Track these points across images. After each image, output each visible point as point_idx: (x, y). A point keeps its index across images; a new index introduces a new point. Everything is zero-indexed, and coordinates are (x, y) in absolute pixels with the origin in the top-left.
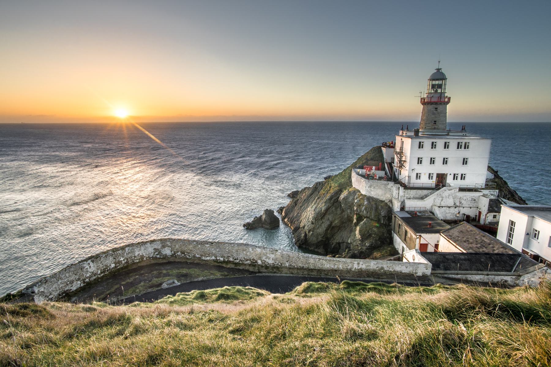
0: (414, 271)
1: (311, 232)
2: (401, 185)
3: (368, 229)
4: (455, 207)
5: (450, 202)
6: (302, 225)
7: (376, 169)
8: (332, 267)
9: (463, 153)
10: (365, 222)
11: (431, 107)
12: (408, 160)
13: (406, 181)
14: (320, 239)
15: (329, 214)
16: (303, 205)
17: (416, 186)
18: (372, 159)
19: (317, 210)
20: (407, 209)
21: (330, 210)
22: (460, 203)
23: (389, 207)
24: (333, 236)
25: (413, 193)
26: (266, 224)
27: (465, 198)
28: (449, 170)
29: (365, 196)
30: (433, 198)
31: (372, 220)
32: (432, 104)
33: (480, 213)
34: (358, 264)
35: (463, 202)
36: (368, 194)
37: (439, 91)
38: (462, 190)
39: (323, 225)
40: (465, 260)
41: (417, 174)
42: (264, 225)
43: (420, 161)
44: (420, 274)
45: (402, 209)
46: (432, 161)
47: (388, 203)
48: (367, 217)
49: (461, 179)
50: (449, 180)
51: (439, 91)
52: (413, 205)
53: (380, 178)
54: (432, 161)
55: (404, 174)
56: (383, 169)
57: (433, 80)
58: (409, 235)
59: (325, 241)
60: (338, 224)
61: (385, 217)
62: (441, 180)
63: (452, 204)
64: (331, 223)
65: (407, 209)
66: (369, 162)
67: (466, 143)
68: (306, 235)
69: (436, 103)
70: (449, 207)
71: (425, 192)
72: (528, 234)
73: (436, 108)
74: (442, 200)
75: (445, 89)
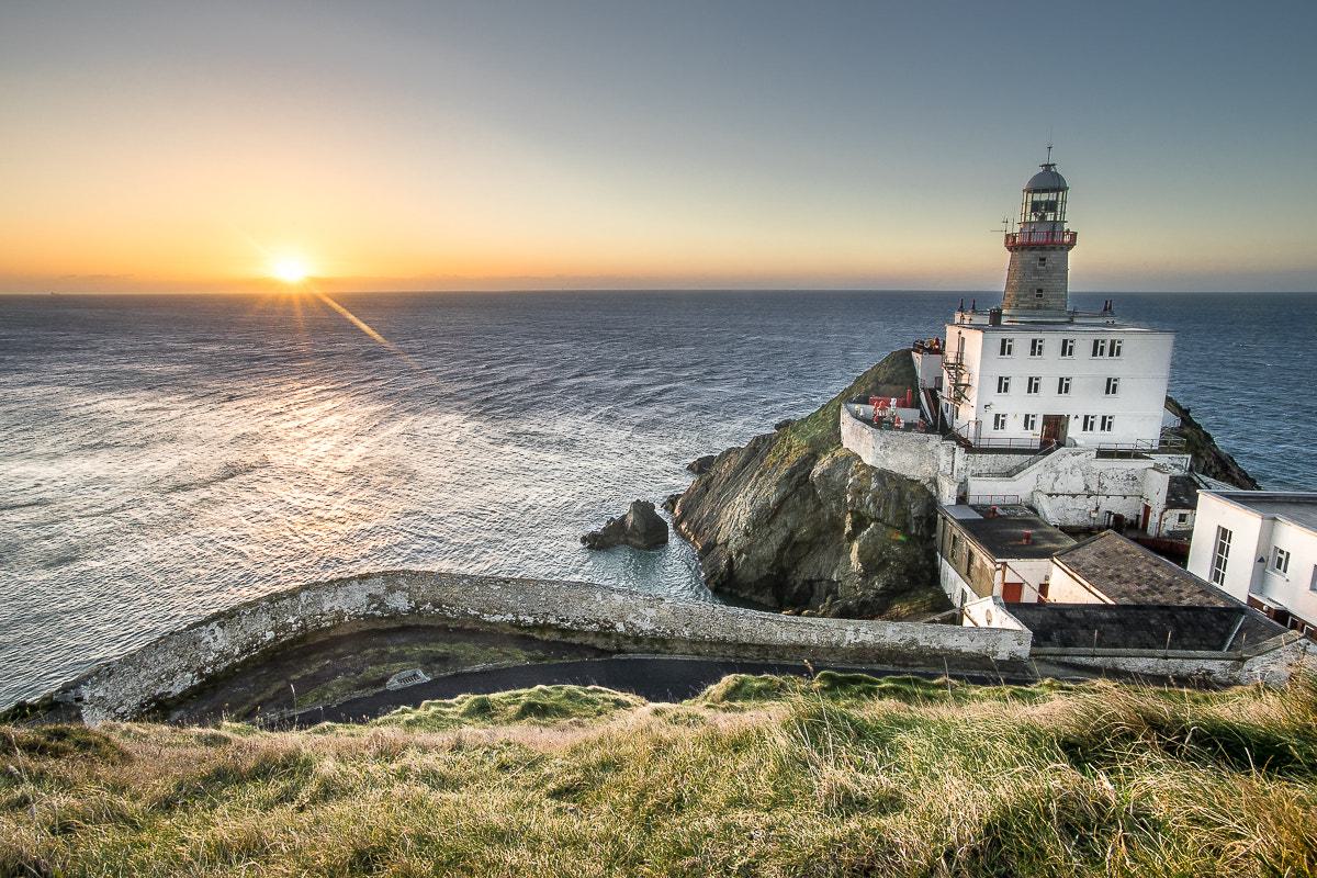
0: (990, 649)
3: (879, 546)
4: (1089, 496)
5: (1076, 483)
6: (721, 538)
7: (898, 405)
9: (1107, 367)
11: (1029, 256)
14: (765, 571)
15: (787, 513)
17: (993, 444)
19: (758, 503)
20: (972, 501)
21: (790, 503)
22: (1100, 485)
25: (986, 461)
26: (635, 536)
30: (1036, 472)
31: (888, 525)
33: (1147, 509)
34: (857, 631)
35: (1107, 482)
36: (879, 465)
38: (1103, 454)
39: (772, 538)
41: (997, 416)
42: (630, 539)
43: (1003, 385)
44: (1003, 655)
45: (962, 499)
46: (1033, 386)
47: (928, 487)
48: (876, 520)
50: (1074, 430)
51: (1050, 217)
52: (987, 490)
53: (909, 427)
54: (1033, 386)
55: (966, 417)
56: (917, 404)
59: (777, 576)
60: (808, 537)
61: (919, 518)
62: (1055, 429)
64: (792, 533)
65: (972, 501)
66: (883, 388)
67: (1113, 343)
68: (731, 563)
69: (1041, 247)
70: (1074, 496)
71: (1016, 459)
72: (1261, 560)
74: (1056, 479)
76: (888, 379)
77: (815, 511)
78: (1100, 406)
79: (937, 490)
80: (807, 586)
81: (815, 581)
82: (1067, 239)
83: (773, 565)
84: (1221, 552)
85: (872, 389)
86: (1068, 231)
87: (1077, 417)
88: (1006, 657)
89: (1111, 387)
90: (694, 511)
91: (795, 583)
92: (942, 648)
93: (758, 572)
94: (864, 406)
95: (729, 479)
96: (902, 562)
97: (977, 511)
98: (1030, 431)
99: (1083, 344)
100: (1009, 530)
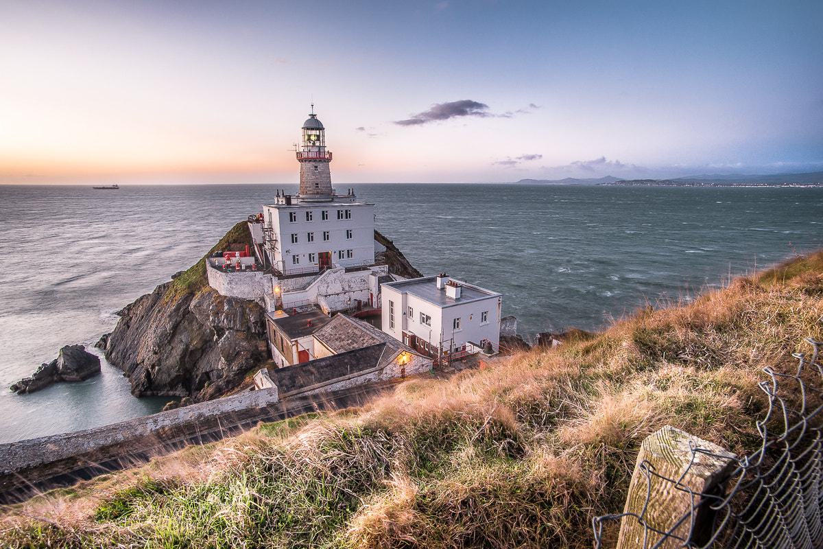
0: (254, 404)
1: (157, 368)
2: (274, 275)
3: (233, 345)
4: (345, 293)
5: (337, 288)
7: (241, 256)
8: (102, 442)
9: (345, 224)
10: (227, 336)
11: (309, 165)
12: (279, 239)
13: (280, 267)
14: (174, 374)
16: (140, 326)
17: (295, 273)
18: (235, 241)
19: (159, 331)
20: (285, 307)
21: (182, 327)
22: (349, 286)
23: (261, 308)
24: (195, 365)
26: (72, 372)
27: (353, 280)
28: (330, 247)
29: (226, 297)
30: (317, 286)
31: (237, 331)
32: (310, 161)
33: (372, 294)
34: (155, 421)
35: (352, 285)
36: (228, 295)
37: (317, 144)
38: (348, 270)
39: (174, 352)
40: (327, 366)
42: (64, 376)
43: (294, 239)
44: (262, 404)
45: (279, 307)
46: (310, 237)
47: (260, 303)
49: (349, 257)
50: (335, 259)
51: (317, 144)
52: (293, 299)
54: (310, 237)
55: (278, 260)
57: (308, 129)
58: (285, 344)
59: (184, 374)
60: (199, 346)
61: (256, 323)
62: (325, 261)
63: (339, 290)
64: (187, 346)
65: (285, 307)
66: (232, 246)
68: (148, 375)
69: (314, 160)
70: (338, 294)
71: (307, 279)
72: (405, 314)
73: (316, 167)
74: (328, 287)
75: (323, 142)
76: (234, 240)
77: (200, 328)
78: (345, 245)
79: (265, 304)
80: (205, 377)
81: (210, 371)
82: (327, 156)
83: (179, 369)
84: (392, 309)
85: (226, 247)
86: (328, 152)
87: (335, 252)
88: (264, 405)
89: (349, 235)
90: (120, 344)
91: (197, 377)
92: (222, 413)
93: (169, 375)
94: (219, 258)
95: (143, 317)
96: (249, 351)
97: (286, 313)
98: (313, 262)
99: (332, 214)
100: (300, 321)
